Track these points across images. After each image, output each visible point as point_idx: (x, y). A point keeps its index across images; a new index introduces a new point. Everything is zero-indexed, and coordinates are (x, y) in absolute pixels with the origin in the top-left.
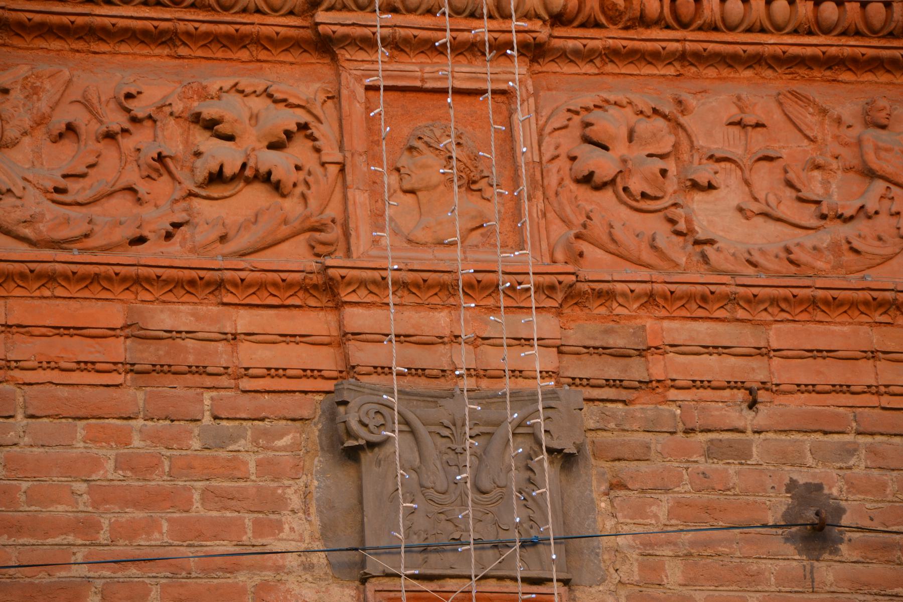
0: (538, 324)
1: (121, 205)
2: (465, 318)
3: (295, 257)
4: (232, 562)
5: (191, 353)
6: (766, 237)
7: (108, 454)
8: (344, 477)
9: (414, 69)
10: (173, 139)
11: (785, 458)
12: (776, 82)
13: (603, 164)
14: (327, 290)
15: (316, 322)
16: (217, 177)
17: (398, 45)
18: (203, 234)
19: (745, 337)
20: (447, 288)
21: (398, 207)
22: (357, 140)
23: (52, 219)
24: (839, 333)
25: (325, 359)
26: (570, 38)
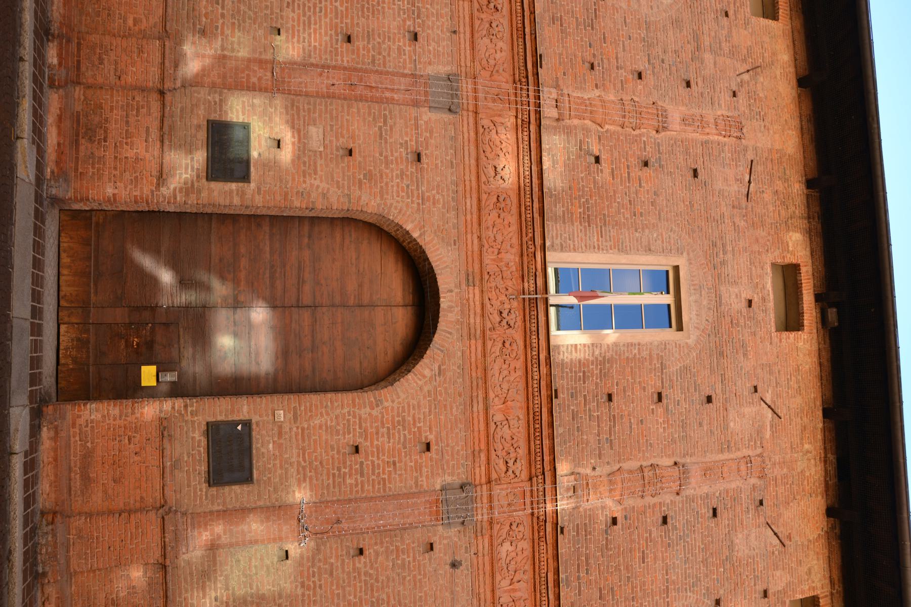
0: (486, 517)
1: (501, 447)
2: (486, 505)
3: (494, 476)
4: (443, 469)
5: (477, 460)
6: (504, 555)
7: (460, 448)
8: (458, 486)
9: (528, 494)
10: (513, 455)
11: (466, 560)
12: (530, 556)
13: (514, 527)
14: (489, 482)
15: (484, 480)
16: (507, 463)
17: (532, 491)
18: (497, 461)
19: (486, 552)
20: (491, 502)
21: (504, 493)
22: (515, 485)
23: (498, 437)
24: (474, 184)
25: (477, 482)
26: (535, 520)
